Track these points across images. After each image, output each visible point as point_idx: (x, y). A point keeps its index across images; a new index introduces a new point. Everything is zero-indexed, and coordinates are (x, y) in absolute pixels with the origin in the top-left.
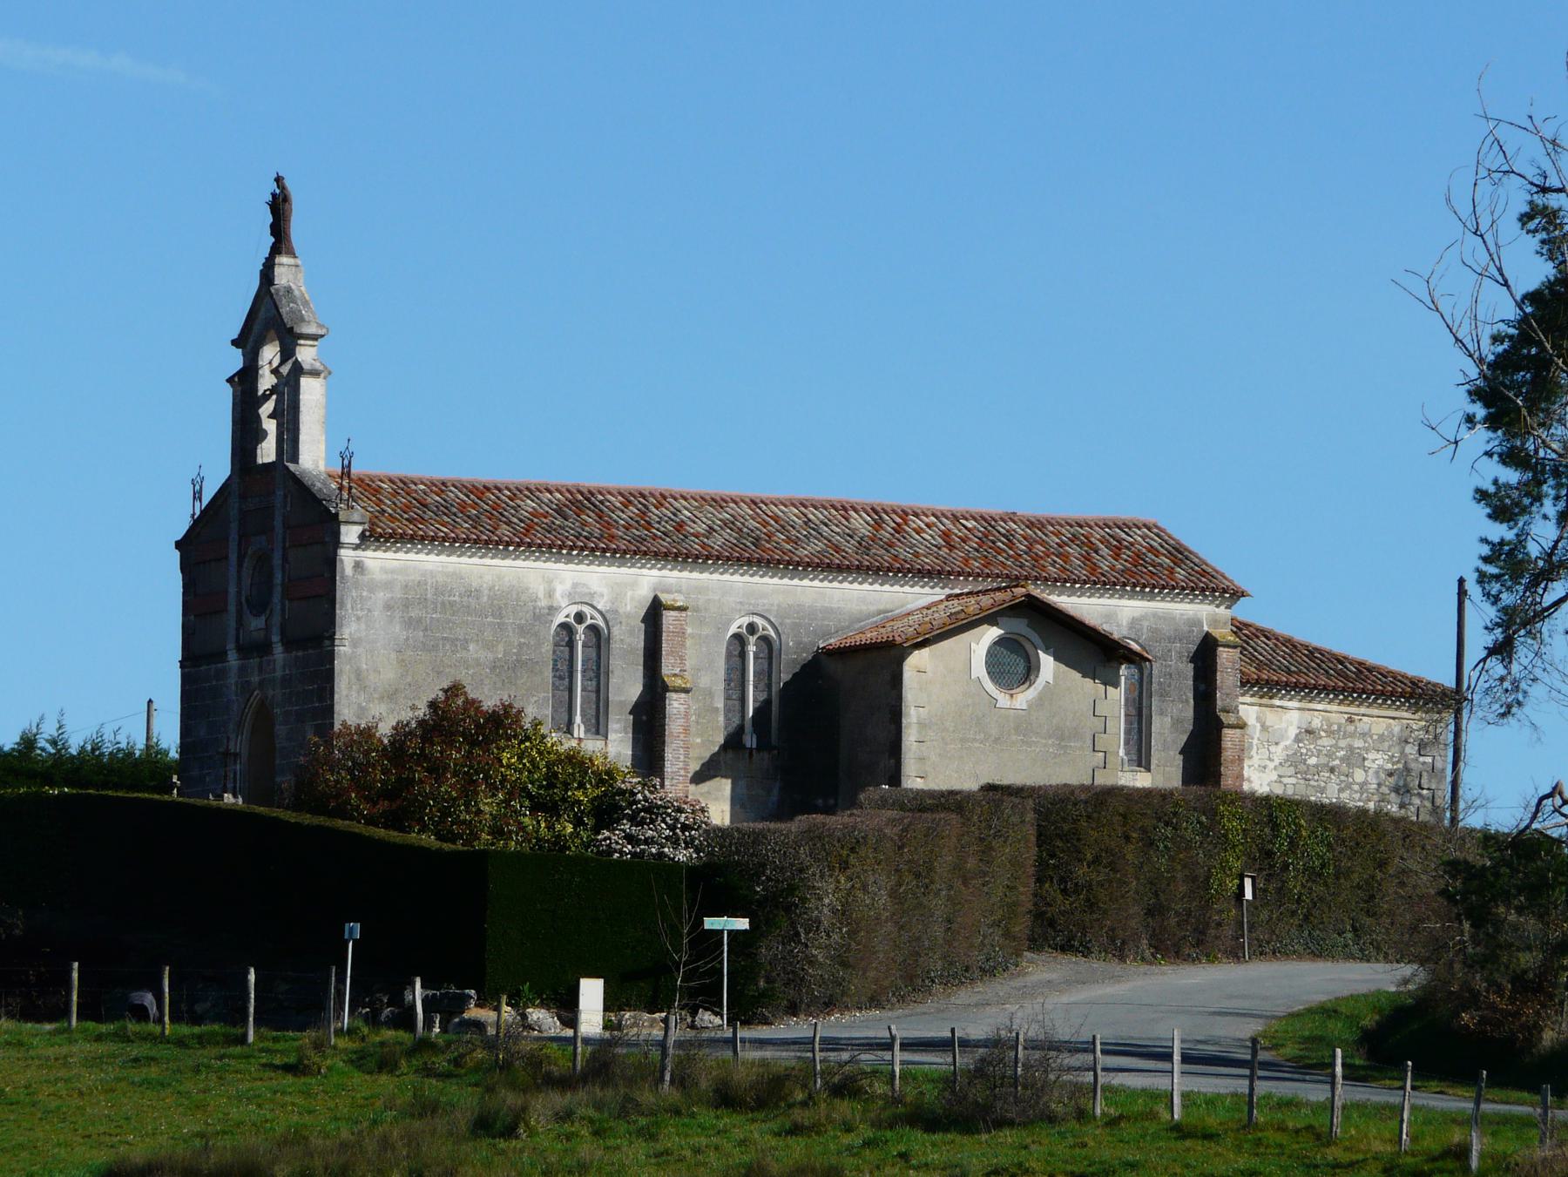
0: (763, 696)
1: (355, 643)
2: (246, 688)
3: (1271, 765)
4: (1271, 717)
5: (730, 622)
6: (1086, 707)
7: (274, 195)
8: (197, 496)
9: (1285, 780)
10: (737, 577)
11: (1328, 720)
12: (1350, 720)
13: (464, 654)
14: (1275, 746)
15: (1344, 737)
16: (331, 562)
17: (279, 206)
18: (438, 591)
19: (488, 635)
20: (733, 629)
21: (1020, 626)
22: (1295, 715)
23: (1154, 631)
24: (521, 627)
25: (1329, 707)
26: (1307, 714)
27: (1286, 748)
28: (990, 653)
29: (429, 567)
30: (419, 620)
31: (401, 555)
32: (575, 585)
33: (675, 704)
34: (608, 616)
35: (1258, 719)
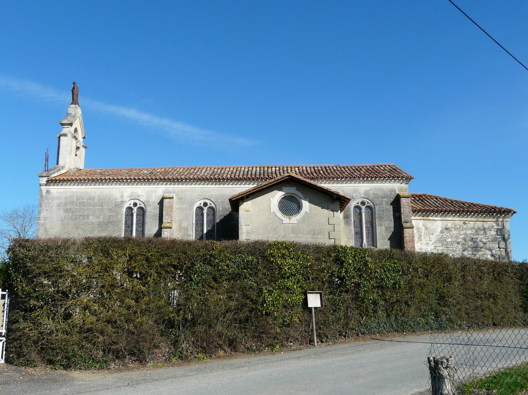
0: (209, 228)
1: (45, 219)
3: (431, 243)
4: (429, 224)
5: (193, 203)
6: (325, 221)
9: (438, 248)
10: (197, 186)
11: (454, 224)
12: (465, 224)
13: (87, 220)
14: (428, 236)
15: (463, 230)
18: (78, 198)
19: (97, 213)
20: (197, 205)
21: (293, 190)
22: (440, 222)
23: (375, 195)
24: (110, 210)
25: (454, 219)
26: (445, 222)
27: (437, 236)
28: (281, 202)
29: (75, 190)
30: (70, 209)
31: (63, 187)
32: (132, 193)
33: (166, 233)
34: (145, 203)
35: (423, 225)
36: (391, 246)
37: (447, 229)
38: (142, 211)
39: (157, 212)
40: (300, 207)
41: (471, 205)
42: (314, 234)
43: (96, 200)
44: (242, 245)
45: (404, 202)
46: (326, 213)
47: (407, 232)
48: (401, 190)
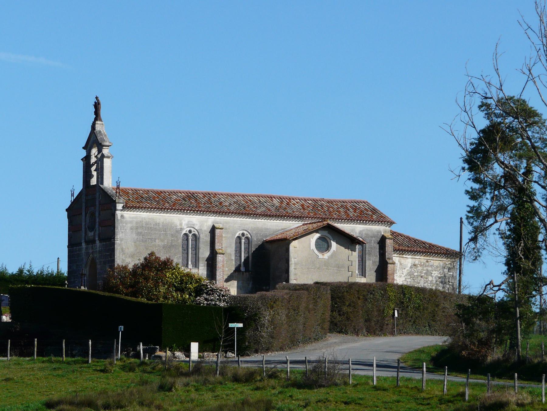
0: (247, 255)
1: (121, 240)
2: (88, 254)
3: (403, 275)
4: (403, 261)
7: (95, 102)
8: (72, 195)
10: (238, 219)
12: (427, 262)
14: (404, 270)
16: (114, 215)
17: (97, 106)
20: (237, 235)
21: (326, 233)
22: (410, 259)
24: (172, 235)
27: (408, 270)
29: (144, 216)
30: (141, 233)
32: (189, 222)
33: (220, 258)
35: (399, 261)
36: (377, 280)
37: (415, 265)
38: (196, 238)
39: (208, 239)
40: (328, 247)
41: (431, 246)
42: (339, 267)
43: (161, 226)
44: (389, 284)
45: (389, 242)
46: (347, 252)
47: (390, 267)
48: (385, 232)
